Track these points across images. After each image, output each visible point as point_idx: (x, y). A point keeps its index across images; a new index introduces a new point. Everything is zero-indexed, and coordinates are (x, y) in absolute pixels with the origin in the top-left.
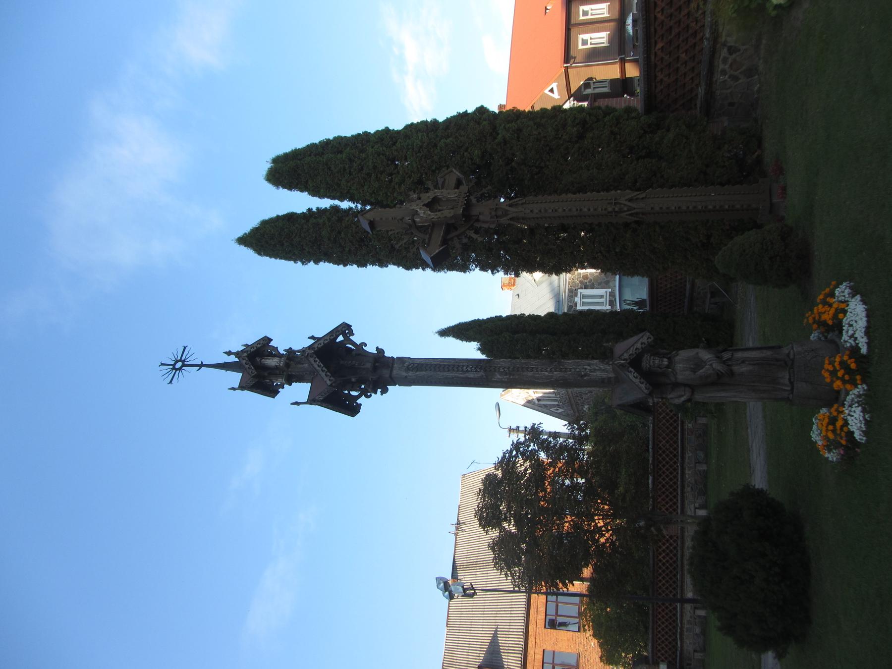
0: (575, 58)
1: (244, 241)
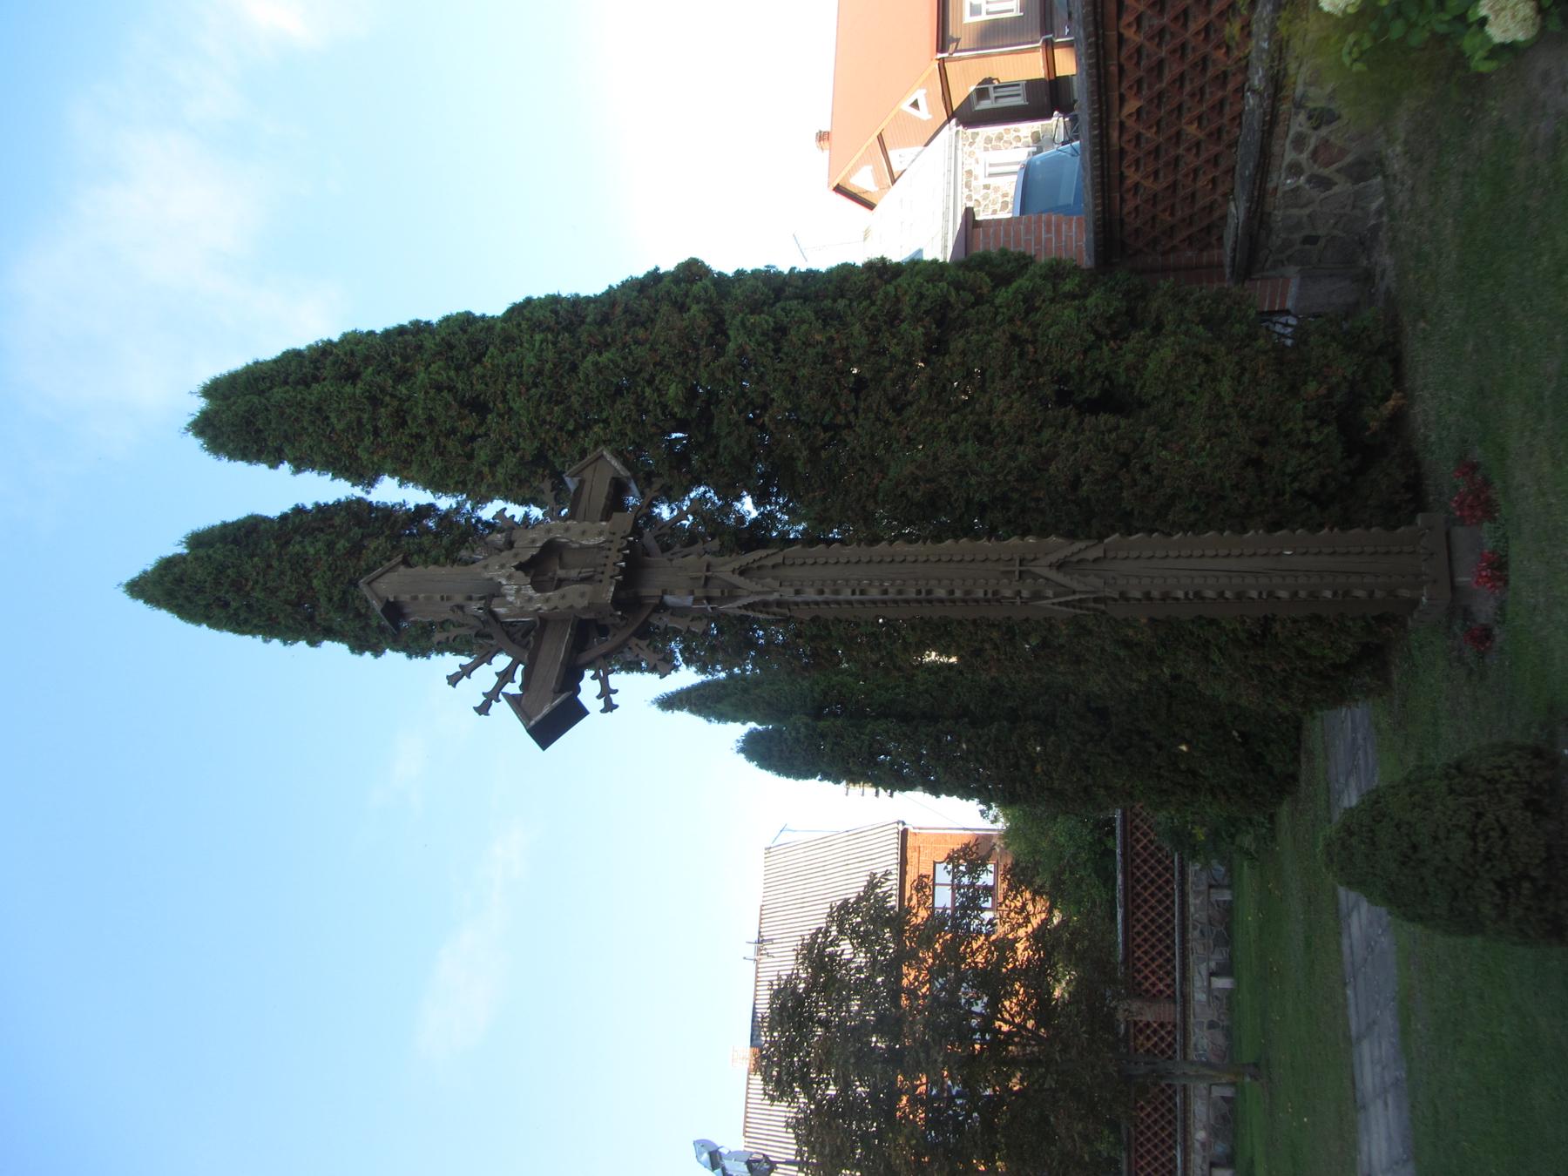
0: (958, 40)
1: (142, 588)
